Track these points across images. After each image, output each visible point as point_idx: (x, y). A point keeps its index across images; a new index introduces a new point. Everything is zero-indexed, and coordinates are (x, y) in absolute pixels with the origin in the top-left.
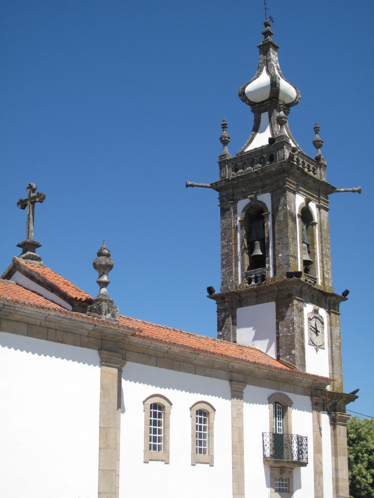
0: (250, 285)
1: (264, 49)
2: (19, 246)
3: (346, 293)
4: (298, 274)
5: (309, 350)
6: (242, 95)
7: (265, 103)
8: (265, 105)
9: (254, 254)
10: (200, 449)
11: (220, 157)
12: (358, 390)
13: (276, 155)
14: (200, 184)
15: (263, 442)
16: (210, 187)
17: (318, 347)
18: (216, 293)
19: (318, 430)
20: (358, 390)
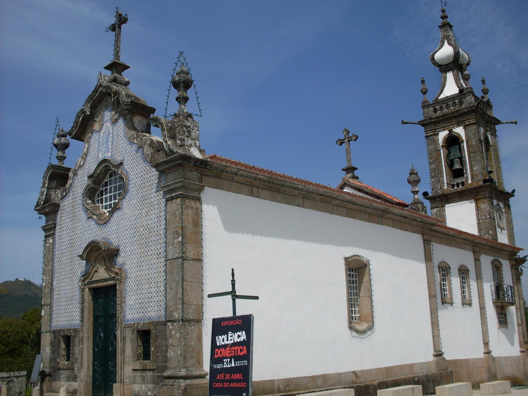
0: (454, 189)
2: (344, 170)
3: (514, 191)
7: (449, 65)
8: (450, 67)
9: (454, 168)
11: (422, 103)
12: (527, 256)
15: (492, 290)
16: (418, 124)
17: (502, 229)
18: (429, 195)
20: (527, 256)
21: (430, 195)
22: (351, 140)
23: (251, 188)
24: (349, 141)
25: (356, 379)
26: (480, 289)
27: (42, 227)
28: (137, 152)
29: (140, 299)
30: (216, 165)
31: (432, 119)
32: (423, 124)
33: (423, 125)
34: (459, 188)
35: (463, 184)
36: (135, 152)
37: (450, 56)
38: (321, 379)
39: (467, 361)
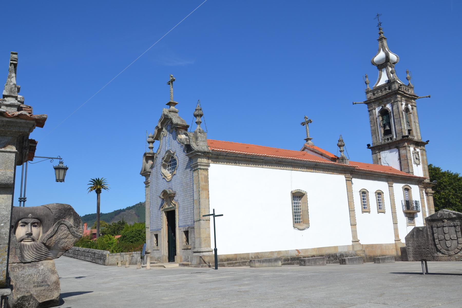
1: (381, 39)
4: (407, 136)
5: (414, 166)
6: (373, 63)
7: (383, 65)
9: (386, 129)
10: (364, 207)
13: (392, 87)
14: (360, 103)
17: (417, 165)
19: (422, 198)
21: (371, 146)
22: (309, 123)
23: (235, 161)
24: (307, 123)
25: (298, 254)
26: (392, 203)
27: (144, 182)
28: (181, 147)
29: (184, 216)
30: (215, 153)
31: (371, 100)
32: (366, 103)
33: (366, 104)
34: (389, 141)
35: (391, 139)
36: (180, 148)
37: (383, 59)
38: (276, 253)
39: (381, 245)
